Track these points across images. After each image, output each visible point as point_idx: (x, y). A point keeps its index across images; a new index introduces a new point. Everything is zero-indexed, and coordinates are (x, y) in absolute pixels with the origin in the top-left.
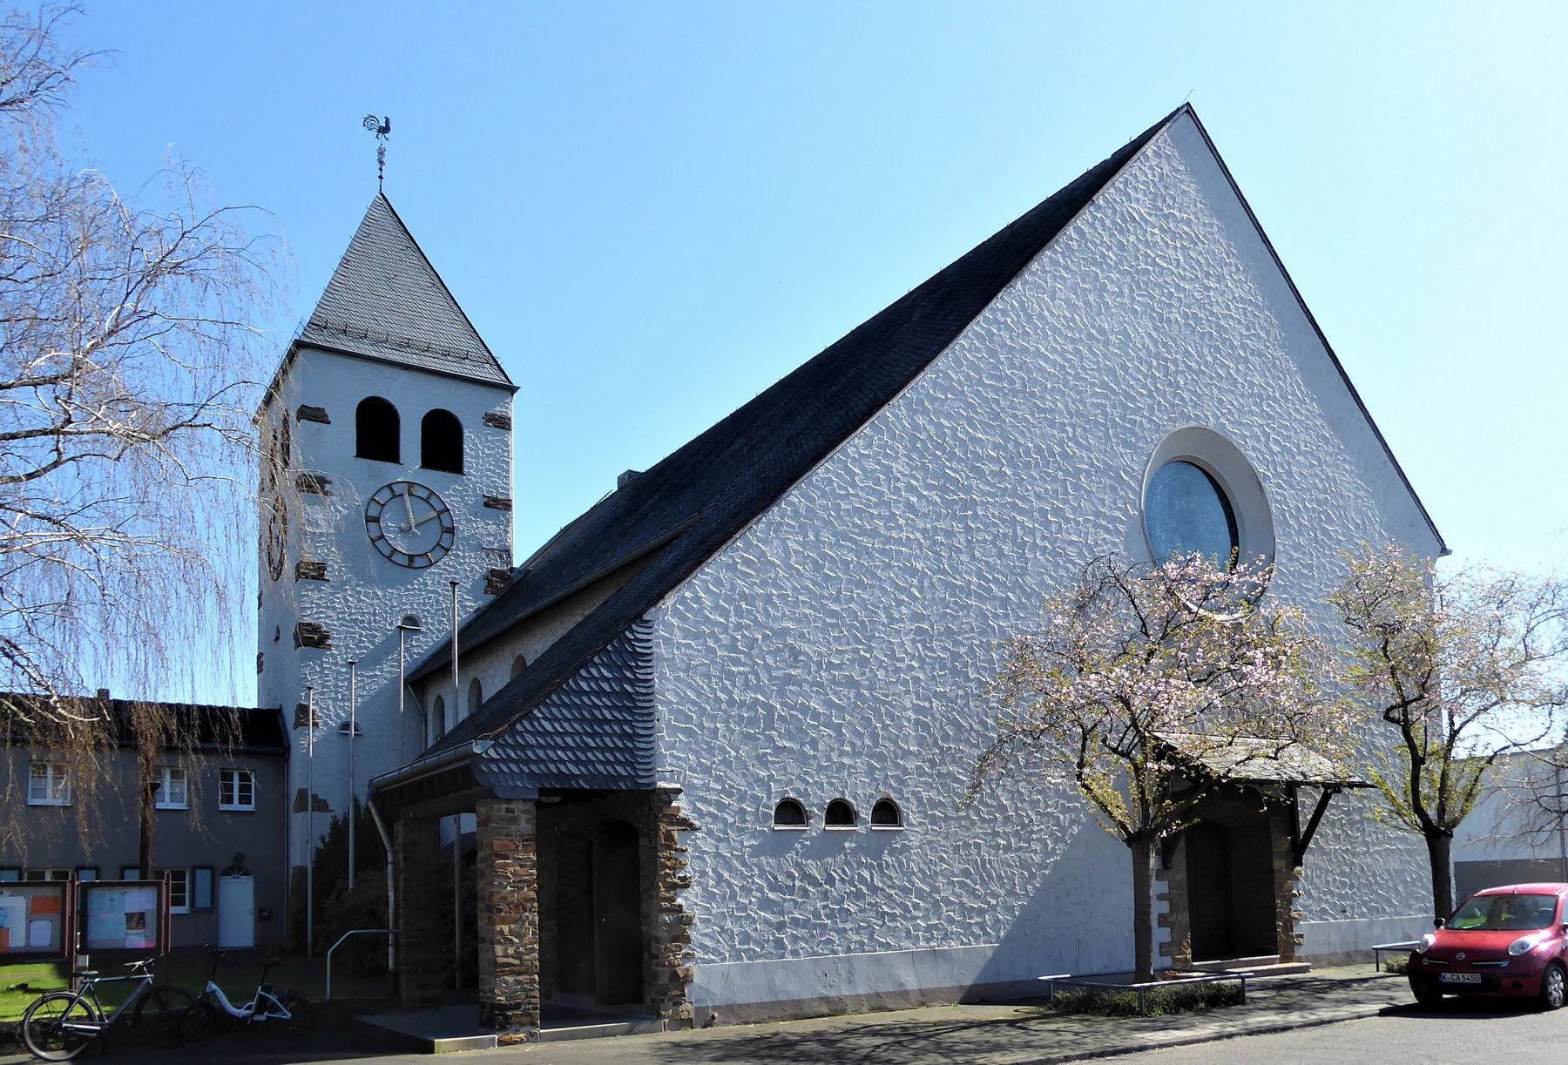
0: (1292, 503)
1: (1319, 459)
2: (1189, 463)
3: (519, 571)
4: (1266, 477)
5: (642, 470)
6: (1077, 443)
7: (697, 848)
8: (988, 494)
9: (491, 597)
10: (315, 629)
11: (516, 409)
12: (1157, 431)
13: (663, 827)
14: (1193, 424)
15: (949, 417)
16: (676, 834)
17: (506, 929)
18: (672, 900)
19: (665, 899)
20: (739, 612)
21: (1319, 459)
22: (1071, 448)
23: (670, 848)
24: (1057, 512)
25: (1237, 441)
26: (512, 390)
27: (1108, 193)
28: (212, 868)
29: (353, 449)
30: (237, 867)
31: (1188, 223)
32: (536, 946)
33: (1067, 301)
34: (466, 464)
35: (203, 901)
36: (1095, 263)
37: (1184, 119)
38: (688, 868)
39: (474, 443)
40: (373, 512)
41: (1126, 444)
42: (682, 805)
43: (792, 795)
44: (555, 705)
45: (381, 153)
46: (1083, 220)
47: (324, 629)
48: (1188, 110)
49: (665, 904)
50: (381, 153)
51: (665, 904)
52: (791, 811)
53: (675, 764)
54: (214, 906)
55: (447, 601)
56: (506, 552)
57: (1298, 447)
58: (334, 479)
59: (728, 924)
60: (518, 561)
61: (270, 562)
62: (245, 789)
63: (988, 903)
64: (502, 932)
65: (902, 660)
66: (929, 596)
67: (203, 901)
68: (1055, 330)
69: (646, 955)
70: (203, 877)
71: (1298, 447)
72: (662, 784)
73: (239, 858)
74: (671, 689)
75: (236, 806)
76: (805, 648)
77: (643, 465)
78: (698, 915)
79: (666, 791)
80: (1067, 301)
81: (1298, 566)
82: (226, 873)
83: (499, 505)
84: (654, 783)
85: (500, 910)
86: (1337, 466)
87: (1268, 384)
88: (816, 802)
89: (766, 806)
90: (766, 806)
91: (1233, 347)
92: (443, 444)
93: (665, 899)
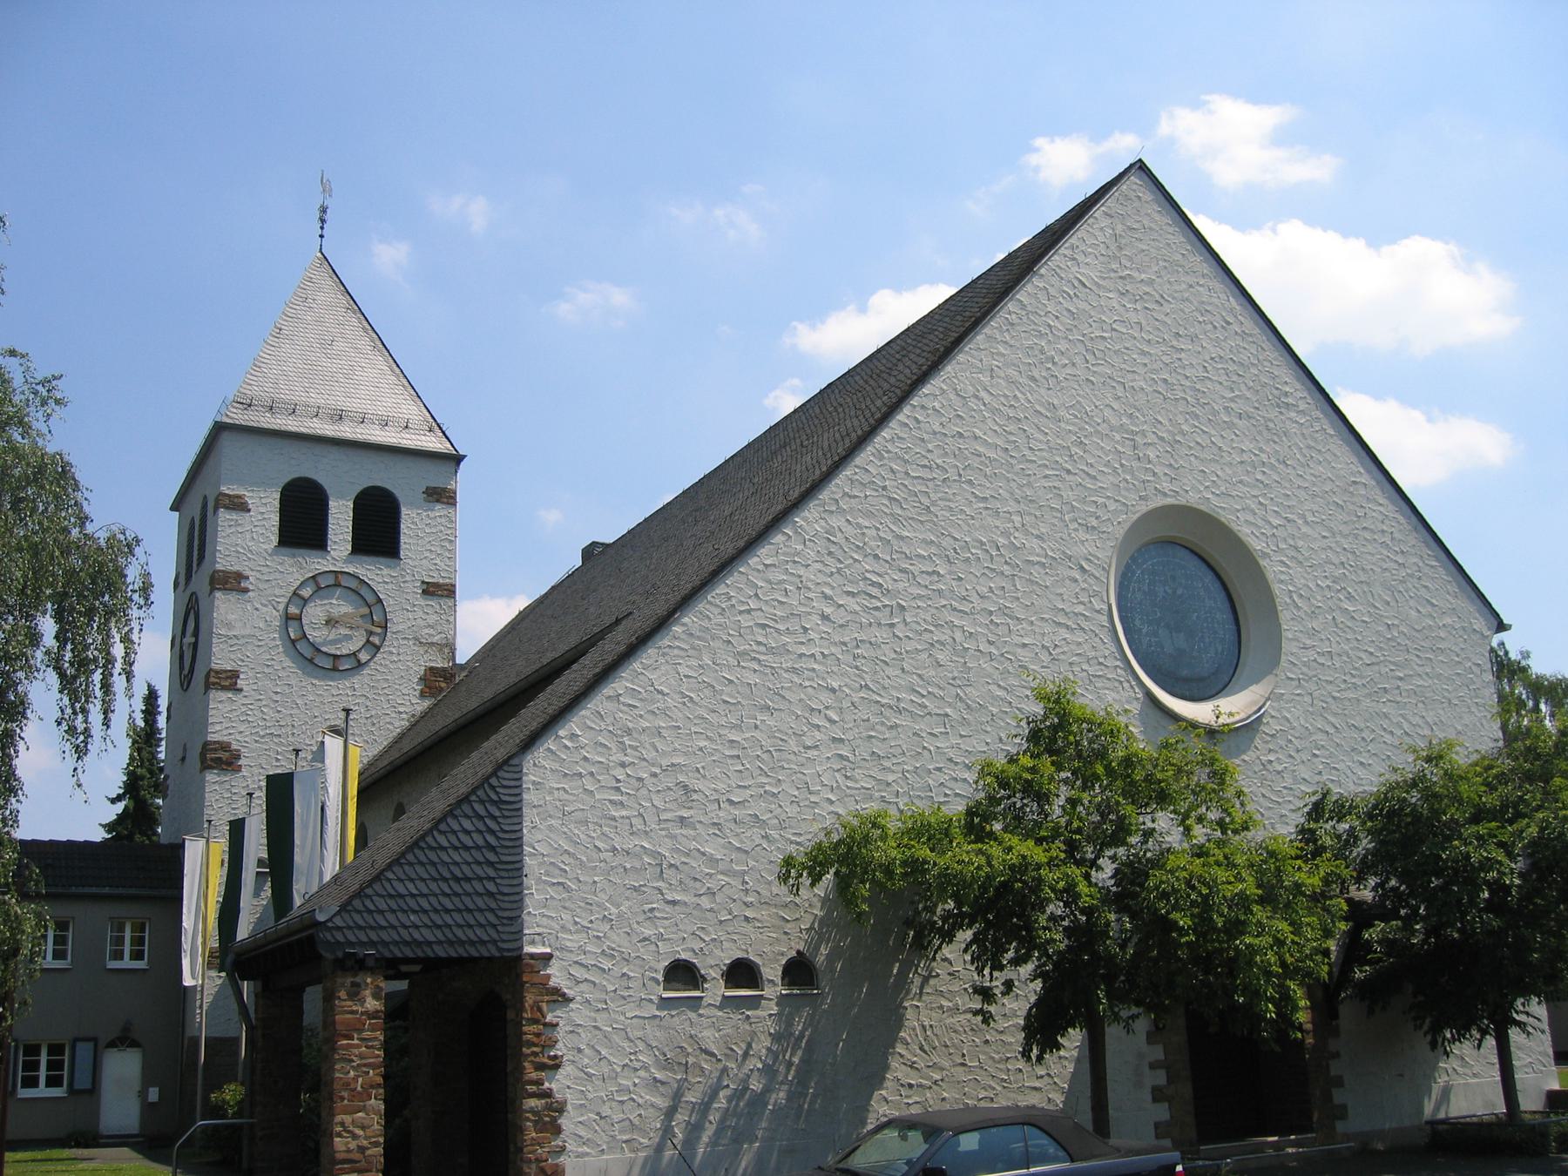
0: (1300, 582)
1: (1330, 529)
2: (1172, 542)
3: (462, 667)
4: (1265, 555)
5: (610, 539)
6: (1027, 533)
7: (570, 1021)
8: (920, 597)
9: (427, 703)
10: (225, 747)
11: (464, 482)
12: (1123, 508)
13: (529, 999)
14: (1169, 501)
15: (869, 514)
16: (544, 1006)
17: (347, 1119)
18: (539, 1083)
19: (532, 1082)
20: (623, 748)
21: (1330, 529)
22: (1019, 539)
23: (536, 1021)
24: (1003, 611)
25: (1226, 517)
26: (457, 459)
27: (1057, 259)
28: (95, 1040)
29: (275, 539)
30: (124, 1040)
31: (1151, 282)
32: (381, 1140)
33: (1007, 378)
34: (403, 546)
35: (83, 1082)
36: (1041, 335)
37: (1134, 180)
38: (560, 1045)
39: (414, 523)
40: (293, 610)
41: (1090, 529)
42: (556, 975)
43: (684, 956)
44: (411, 864)
45: (324, 210)
46: (1025, 293)
47: (234, 747)
48: (1140, 167)
49: (531, 1088)
50: (324, 210)
51: (531, 1088)
52: (682, 973)
53: (551, 924)
54: (94, 1090)
55: (390, 703)
56: (450, 648)
57: (1303, 517)
58: (248, 573)
59: (606, 1111)
60: (462, 657)
61: (181, 668)
62: (138, 941)
63: (929, 1078)
64: (342, 1124)
65: (818, 792)
66: (848, 717)
67: (83, 1082)
68: (994, 411)
69: (512, 1148)
70: (85, 1050)
71: (1303, 517)
72: (529, 949)
73: (126, 1028)
74: (545, 836)
75: (127, 963)
76: (698, 785)
77: (610, 534)
78: (572, 1100)
79: (532, 956)
80: (1007, 378)
81: (1312, 655)
82: (112, 1044)
83: (441, 591)
84: (521, 948)
85: (343, 1099)
86: (1356, 536)
87: (1261, 450)
88: (712, 966)
89: (651, 969)
90: (651, 969)
91: (1215, 413)
92: (378, 529)
93: (532, 1082)
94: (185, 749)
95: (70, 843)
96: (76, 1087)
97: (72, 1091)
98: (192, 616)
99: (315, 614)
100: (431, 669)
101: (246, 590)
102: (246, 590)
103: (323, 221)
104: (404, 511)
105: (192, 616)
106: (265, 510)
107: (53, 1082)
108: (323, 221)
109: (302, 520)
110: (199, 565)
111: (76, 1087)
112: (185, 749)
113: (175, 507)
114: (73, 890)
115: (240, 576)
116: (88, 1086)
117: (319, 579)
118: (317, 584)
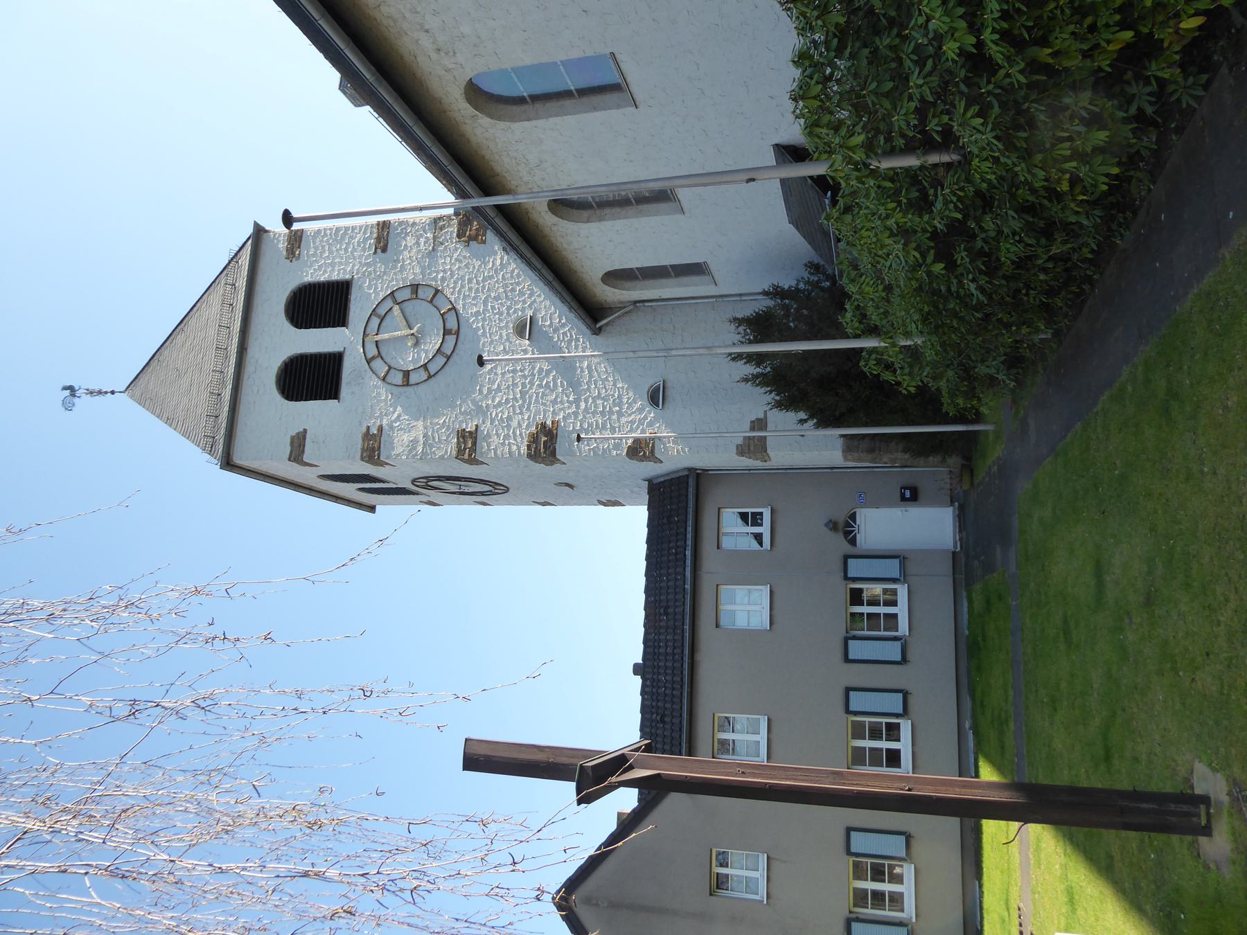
10: (534, 439)
28: (846, 558)
30: (847, 528)
54: (900, 557)
70: (856, 567)
73: (833, 526)
82: (853, 542)
92: (321, 304)
94: (560, 484)
95: (648, 591)
96: (900, 711)
97: (905, 713)
98: (487, 488)
99: (409, 359)
100: (459, 236)
101: (381, 429)
102: (381, 429)
103: (100, 392)
104: (308, 279)
105: (487, 488)
106: (312, 413)
107: (893, 732)
108: (100, 392)
109: (311, 379)
110: (383, 482)
111: (900, 711)
112: (560, 484)
113: (372, 509)
114: (688, 586)
115: (367, 435)
116: (896, 563)
117: (369, 356)
118: (373, 358)
